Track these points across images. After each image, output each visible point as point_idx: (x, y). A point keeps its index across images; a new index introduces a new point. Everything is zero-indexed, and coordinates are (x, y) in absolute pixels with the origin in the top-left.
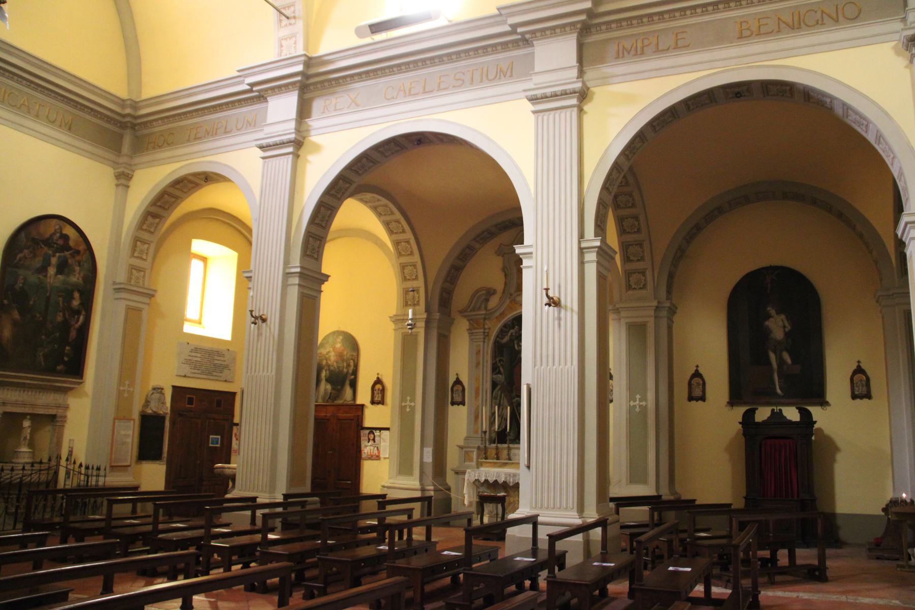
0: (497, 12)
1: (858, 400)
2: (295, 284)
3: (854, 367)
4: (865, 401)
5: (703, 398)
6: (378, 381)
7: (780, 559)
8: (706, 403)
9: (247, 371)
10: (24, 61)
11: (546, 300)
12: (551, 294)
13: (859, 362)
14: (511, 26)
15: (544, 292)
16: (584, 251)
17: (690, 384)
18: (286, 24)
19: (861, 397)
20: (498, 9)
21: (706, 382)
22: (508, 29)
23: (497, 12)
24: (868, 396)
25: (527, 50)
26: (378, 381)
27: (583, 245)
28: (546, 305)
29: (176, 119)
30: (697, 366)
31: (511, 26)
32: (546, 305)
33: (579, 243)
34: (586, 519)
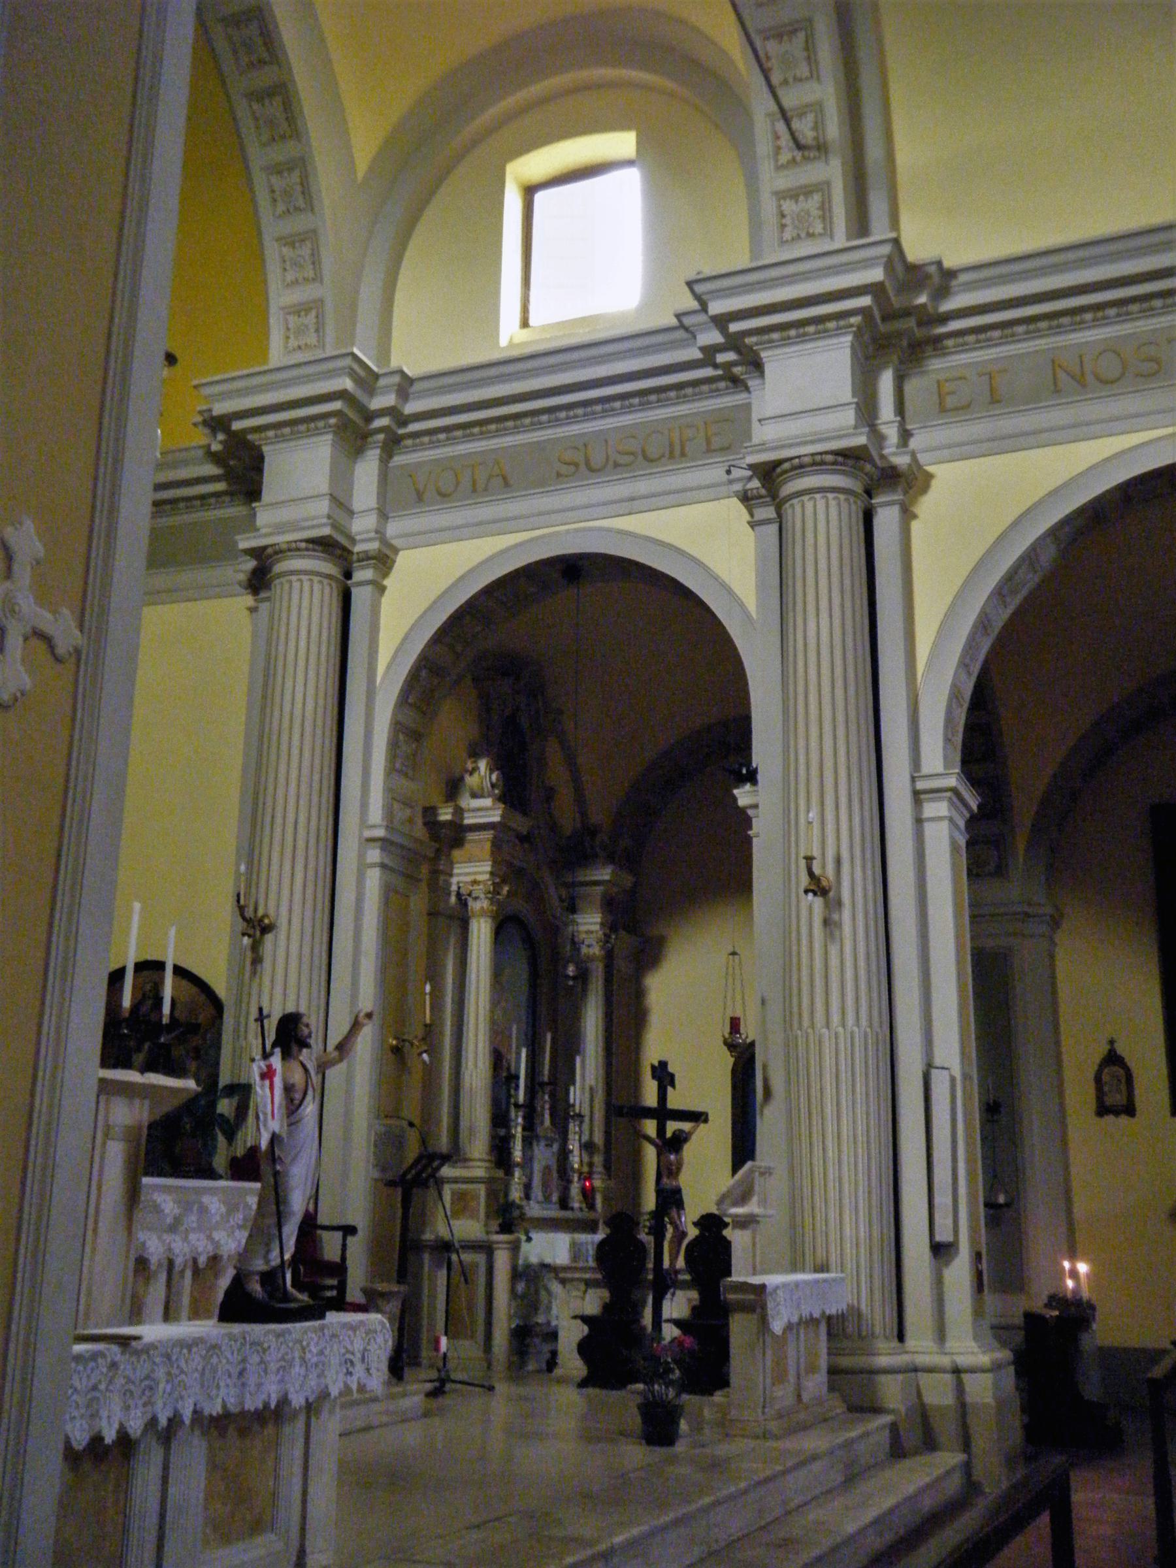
0: (674, 322)
1: (1110, 1119)
2: (940, 819)
3: (1102, 1050)
4: (1124, 1120)
5: (1129, 1110)
6: (1113, 1059)
7: (264, 1397)
8: (1136, 1119)
9: (725, 1004)
10: (1012, 281)
11: (804, 880)
12: (817, 870)
13: (1112, 1042)
14: (703, 349)
15: (803, 863)
16: (922, 796)
17: (1098, 1079)
18: (297, 280)
19: (1115, 1111)
20: (678, 316)
21: (1134, 1075)
22: (698, 355)
23: (674, 322)
24: (1129, 1110)
25: (739, 398)
26: (1113, 1059)
27: (920, 785)
28: (806, 892)
29: (317, 429)
30: (1112, 1042)
31: (703, 349)
32: (806, 892)
33: (913, 779)
34: (916, 1356)
